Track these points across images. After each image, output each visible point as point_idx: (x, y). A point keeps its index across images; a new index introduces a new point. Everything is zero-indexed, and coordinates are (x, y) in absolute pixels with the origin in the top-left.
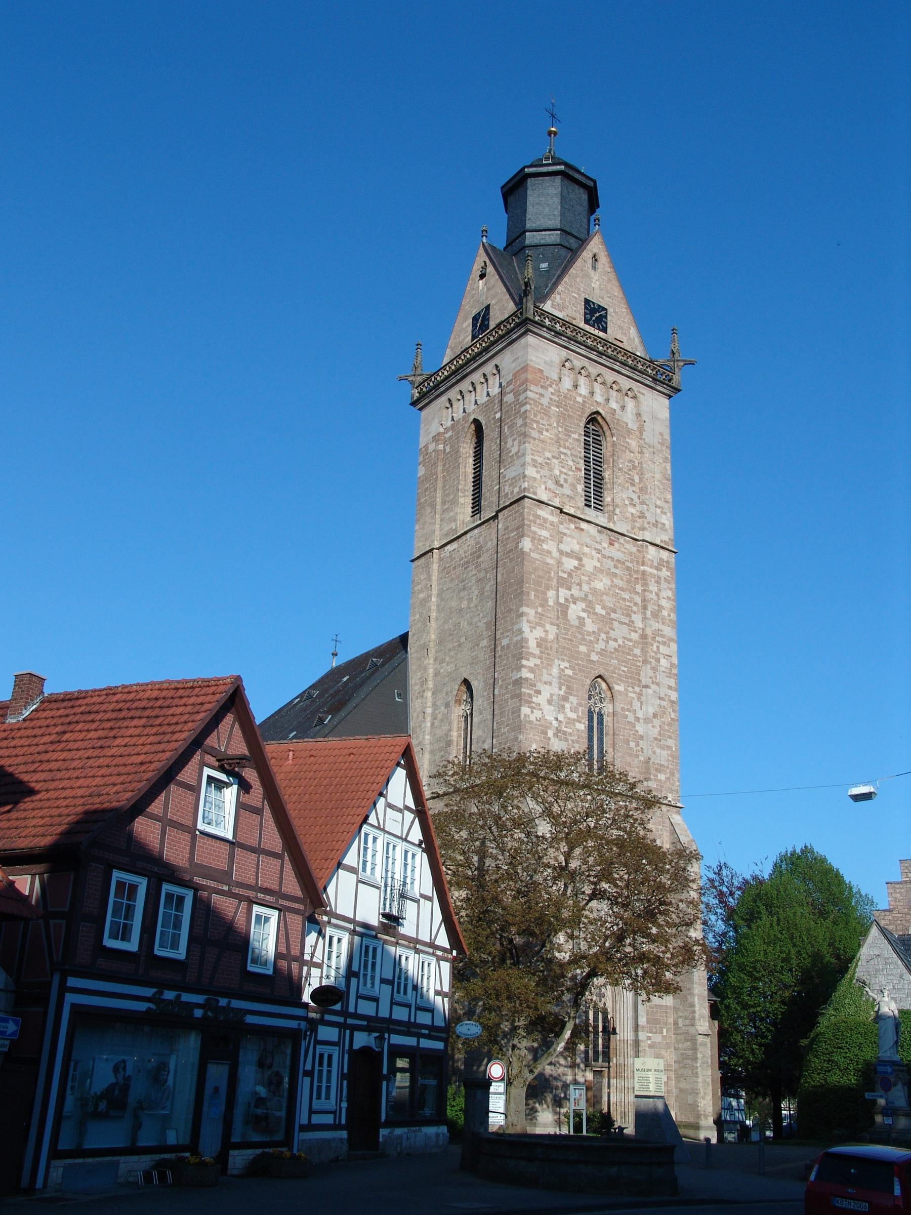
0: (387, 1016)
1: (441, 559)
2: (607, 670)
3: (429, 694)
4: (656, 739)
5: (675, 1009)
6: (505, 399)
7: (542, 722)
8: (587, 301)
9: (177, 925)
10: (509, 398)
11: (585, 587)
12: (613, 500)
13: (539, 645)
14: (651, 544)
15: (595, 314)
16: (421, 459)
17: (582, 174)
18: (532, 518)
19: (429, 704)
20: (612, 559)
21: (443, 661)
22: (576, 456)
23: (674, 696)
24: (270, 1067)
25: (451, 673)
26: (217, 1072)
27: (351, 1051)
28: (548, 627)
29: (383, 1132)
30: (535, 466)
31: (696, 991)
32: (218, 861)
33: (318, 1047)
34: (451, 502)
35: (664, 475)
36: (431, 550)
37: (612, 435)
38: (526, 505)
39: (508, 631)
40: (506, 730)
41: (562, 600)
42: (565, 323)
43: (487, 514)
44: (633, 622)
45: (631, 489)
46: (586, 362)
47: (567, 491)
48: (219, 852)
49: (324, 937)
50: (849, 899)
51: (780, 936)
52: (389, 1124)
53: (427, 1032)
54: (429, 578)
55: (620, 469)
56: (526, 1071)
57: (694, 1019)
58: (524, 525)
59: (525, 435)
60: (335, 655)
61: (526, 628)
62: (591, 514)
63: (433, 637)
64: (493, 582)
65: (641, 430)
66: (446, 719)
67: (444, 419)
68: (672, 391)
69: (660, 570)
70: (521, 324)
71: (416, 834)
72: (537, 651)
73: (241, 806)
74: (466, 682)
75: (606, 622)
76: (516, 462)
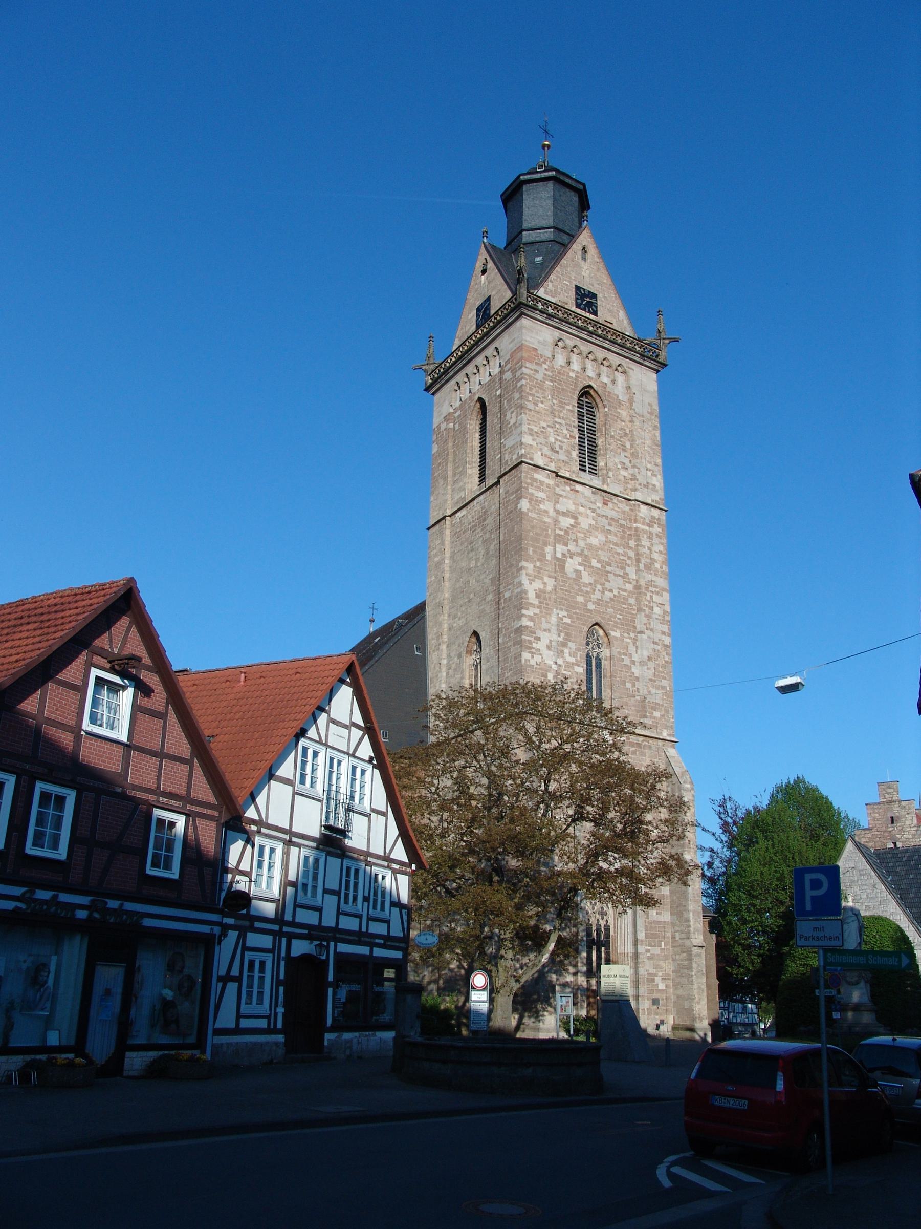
0: (333, 925)
1: (453, 525)
3: (444, 647)
4: (651, 680)
5: (673, 924)
6: (504, 377)
7: (542, 666)
8: (578, 288)
9: (58, 825)
10: (508, 375)
11: (581, 543)
12: (606, 464)
13: (538, 596)
14: (642, 503)
15: (586, 299)
16: (434, 438)
17: (574, 180)
18: (529, 481)
19: (444, 656)
20: (607, 517)
22: (570, 426)
23: (667, 640)
24: (181, 972)
25: (462, 627)
26: (110, 976)
27: (289, 959)
28: (546, 579)
29: (329, 1037)
30: (532, 435)
31: (691, 908)
32: (109, 763)
33: (246, 953)
34: (460, 474)
35: (653, 441)
36: (444, 518)
37: (604, 406)
38: (523, 469)
41: (559, 555)
42: (556, 307)
43: (490, 481)
44: (627, 574)
45: (623, 454)
46: (578, 342)
47: (562, 456)
48: (100, 751)
49: (253, 846)
50: (838, 824)
51: (774, 858)
52: (332, 1029)
53: (382, 941)
54: (443, 543)
55: (612, 436)
56: (513, 980)
57: (689, 932)
58: (522, 487)
59: (521, 407)
60: (372, 621)
61: (525, 580)
62: (586, 477)
63: (447, 595)
64: (496, 542)
65: (631, 401)
66: (459, 668)
68: (660, 366)
69: (652, 527)
70: (516, 309)
71: (366, 750)
72: (536, 602)
73: (136, 709)
74: (475, 634)
75: (602, 574)
76: (514, 432)
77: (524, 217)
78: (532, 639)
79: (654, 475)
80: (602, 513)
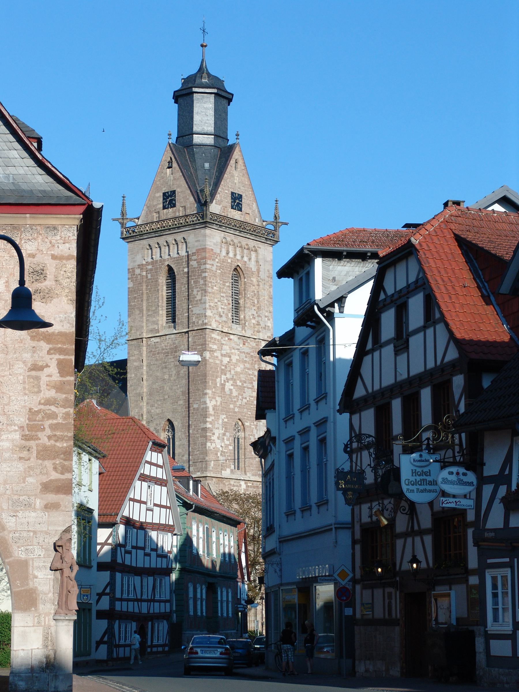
2: (242, 415)
7: (216, 449)
8: (232, 193)
11: (233, 372)
12: (245, 317)
13: (214, 409)
18: (209, 340)
21: (152, 406)
28: (217, 398)
38: (207, 333)
39: (198, 400)
40: (198, 453)
41: (223, 382)
45: (253, 308)
54: (141, 354)
55: (248, 298)
61: (208, 401)
62: (237, 329)
63: (145, 390)
65: (258, 271)
67: (146, 256)
74: (170, 422)
77: (195, 123)
78: (211, 434)
79: (269, 319)
80: (242, 351)
